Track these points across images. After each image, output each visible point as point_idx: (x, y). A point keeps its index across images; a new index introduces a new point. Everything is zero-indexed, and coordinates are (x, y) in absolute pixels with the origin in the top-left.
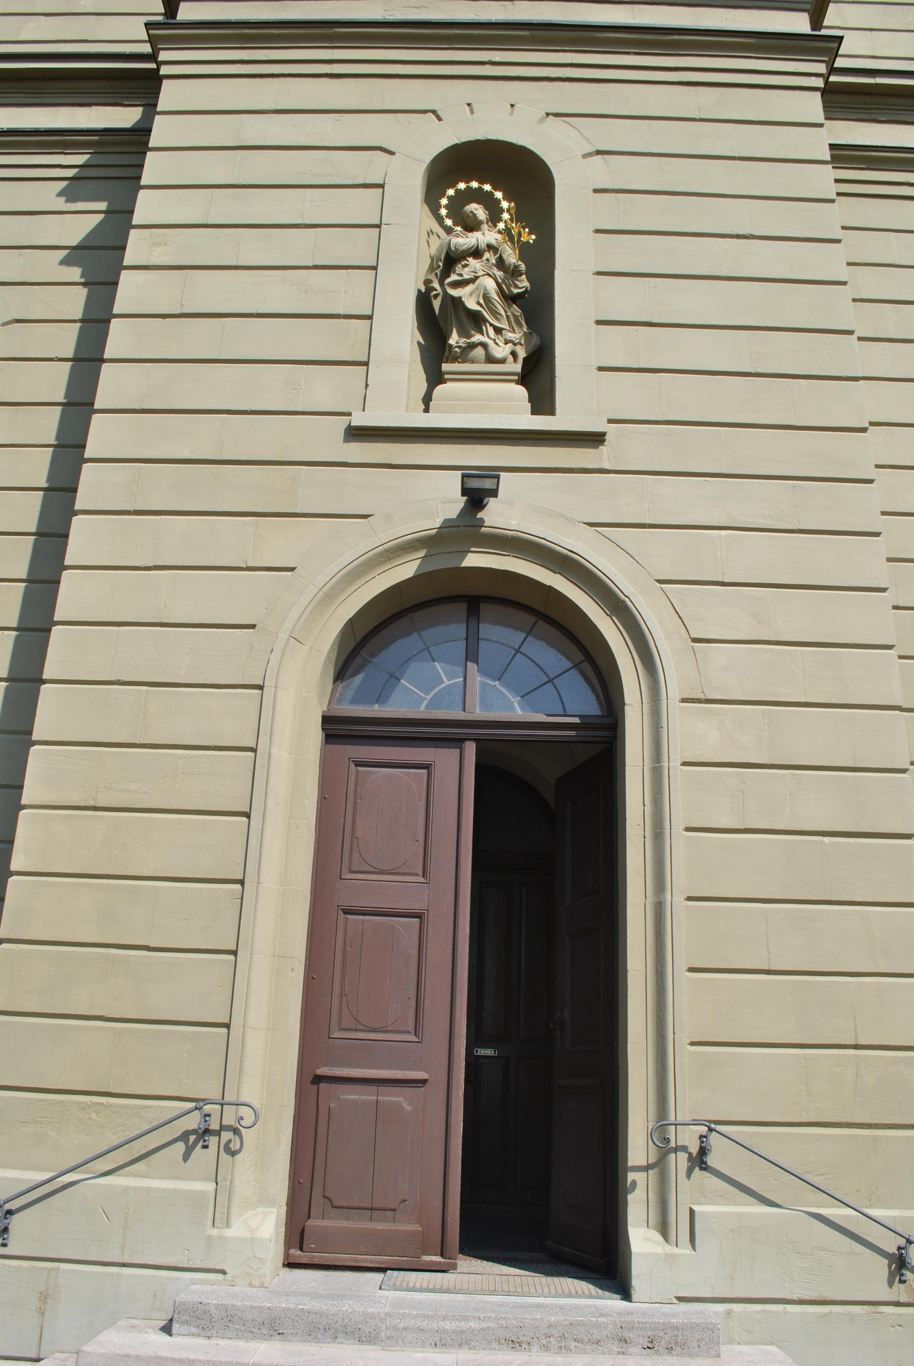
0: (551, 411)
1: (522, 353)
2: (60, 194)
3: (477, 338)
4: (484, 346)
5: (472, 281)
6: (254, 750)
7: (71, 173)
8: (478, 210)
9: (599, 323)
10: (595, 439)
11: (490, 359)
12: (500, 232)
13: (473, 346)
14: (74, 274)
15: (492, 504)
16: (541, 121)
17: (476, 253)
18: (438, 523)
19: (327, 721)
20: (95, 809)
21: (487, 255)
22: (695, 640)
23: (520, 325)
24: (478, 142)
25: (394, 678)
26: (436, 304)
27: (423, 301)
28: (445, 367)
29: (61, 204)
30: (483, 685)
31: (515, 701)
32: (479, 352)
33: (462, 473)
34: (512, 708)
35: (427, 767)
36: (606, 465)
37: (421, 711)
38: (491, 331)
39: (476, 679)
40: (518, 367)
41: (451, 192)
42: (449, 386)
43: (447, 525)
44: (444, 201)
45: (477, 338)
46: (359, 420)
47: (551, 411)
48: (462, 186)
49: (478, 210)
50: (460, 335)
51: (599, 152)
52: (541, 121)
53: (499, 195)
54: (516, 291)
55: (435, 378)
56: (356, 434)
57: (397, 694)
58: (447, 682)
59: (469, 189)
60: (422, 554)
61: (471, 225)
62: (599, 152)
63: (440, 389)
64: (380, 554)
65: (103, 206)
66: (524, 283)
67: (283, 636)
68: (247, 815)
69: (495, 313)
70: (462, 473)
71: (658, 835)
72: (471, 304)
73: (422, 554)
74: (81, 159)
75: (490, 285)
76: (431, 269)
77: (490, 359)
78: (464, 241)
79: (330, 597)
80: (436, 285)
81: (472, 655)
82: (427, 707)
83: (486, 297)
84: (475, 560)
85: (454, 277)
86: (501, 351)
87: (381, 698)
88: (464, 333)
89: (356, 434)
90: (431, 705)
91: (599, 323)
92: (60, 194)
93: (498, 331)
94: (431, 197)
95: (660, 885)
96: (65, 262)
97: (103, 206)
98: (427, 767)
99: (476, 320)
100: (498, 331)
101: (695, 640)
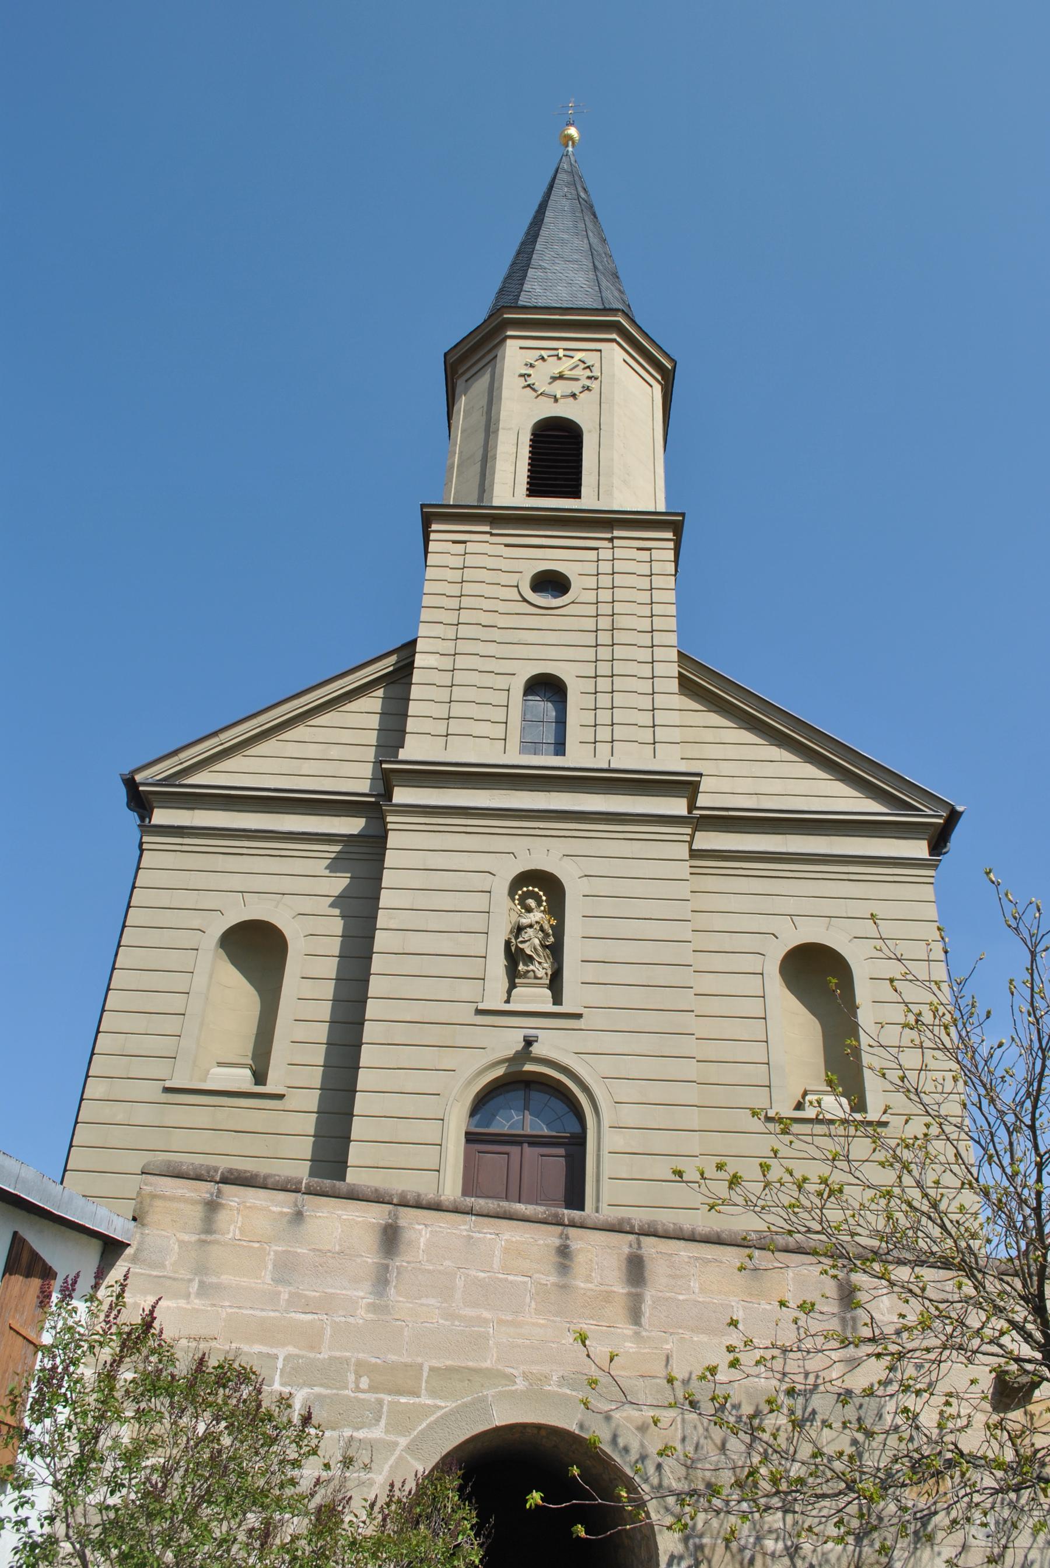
0: (561, 1004)
1: (550, 972)
2: (326, 868)
3: (531, 967)
4: (533, 971)
5: (529, 940)
6: (441, 1145)
7: (333, 855)
8: (531, 902)
9: (582, 961)
10: (579, 1016)
11: (536, 978)
12: (542, 911)
13: (528, 971)
14: (337, 912)
15: (535, 1044)
16: (560, 860)
17: (531, 926)
18: (513, 1052)
19: (467, 1133)
20: (377, 1168)
21: (535, 927)
22: (616, 1103)
23: (549, 958)
24: (532, 870)
25: (494, 1116)
26: (513, 949)
27: (508, 943)
28: (517, 981)
29: (327, 873)
30: (531, 1120)
31: (544, 1127)
32: (531, 974)
33: (576, 494)
34: (543, 1130)
35: (508, 1154)
36: (583, 1028)
37: (505, 1130)
38: (536, 963)
39: (528, 1117)
40: (548, 982)
41: (520, 892)
42: (518, 989)
43: (517, 1053)
44: (517, 897)
45: (531, 967)
46: (481, 1006)
47: (561, 1004)
48: (525, 889)
49: (531, 902)
50: (524, 965)
51: (586, 876)
52: (560, 860)
53: (541, 893)
54: (547, 943)
55: (512, 986)
56: (479, 1012)
57: (495, 1123)
58: (516, 1118)
59: (528, 890)
60: (507, 1065)
61: (529, 910)
62: (586, 876)
63: (515, 991)
64: (490, 1065)
65: (349, 875)
66: (552, 939)
67: (451, 1099)
68: (439, 1171)
69: (538, 955)
70: (576, 494)
71: (598, 1181)
72: (528, 952)
73: (507, 1065)
74: (338, 848)
75: (537, 942)
76: (511, 932)
77: (536, 978)
78: (525, 921)
79: (470, 1082)
80: (513, 940)
81: (526, 1107)
82: (396, 1444)
83: (535, 949)
84: (528, 1067)
85: (521, 939)
86: (541, 973)
87: (488, 1126)
88: (525, 964)
89: (479, 1012)
90: (510, 1127)
91: (582, 961)
92: (326, 868)
93: (540, 963)
94: (512, 893)
95: (598, 1200)
96: (332, 905)
97: (349, 875)
98: (508, 1154)
99: (531, 959)
100: (540, 963)
101: (616, 1103)
